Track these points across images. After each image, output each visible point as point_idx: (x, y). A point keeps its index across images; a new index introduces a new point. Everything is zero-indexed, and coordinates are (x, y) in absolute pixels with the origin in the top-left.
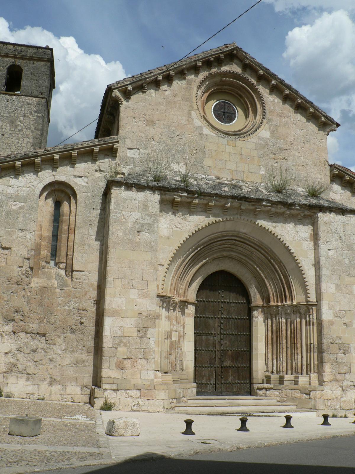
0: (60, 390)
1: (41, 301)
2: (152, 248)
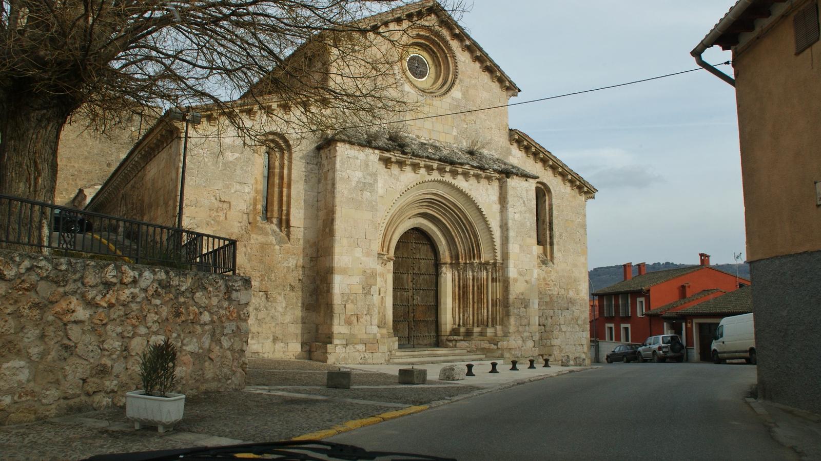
0: (282, 348)
1: (261, 258)
2: (373, 208)
